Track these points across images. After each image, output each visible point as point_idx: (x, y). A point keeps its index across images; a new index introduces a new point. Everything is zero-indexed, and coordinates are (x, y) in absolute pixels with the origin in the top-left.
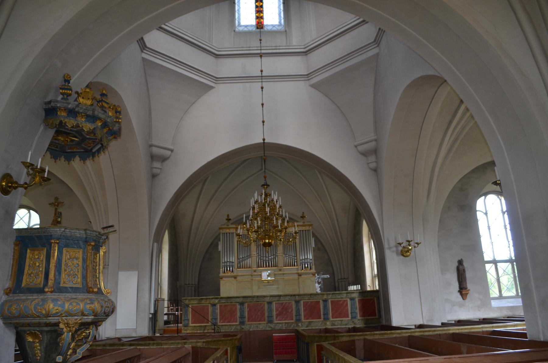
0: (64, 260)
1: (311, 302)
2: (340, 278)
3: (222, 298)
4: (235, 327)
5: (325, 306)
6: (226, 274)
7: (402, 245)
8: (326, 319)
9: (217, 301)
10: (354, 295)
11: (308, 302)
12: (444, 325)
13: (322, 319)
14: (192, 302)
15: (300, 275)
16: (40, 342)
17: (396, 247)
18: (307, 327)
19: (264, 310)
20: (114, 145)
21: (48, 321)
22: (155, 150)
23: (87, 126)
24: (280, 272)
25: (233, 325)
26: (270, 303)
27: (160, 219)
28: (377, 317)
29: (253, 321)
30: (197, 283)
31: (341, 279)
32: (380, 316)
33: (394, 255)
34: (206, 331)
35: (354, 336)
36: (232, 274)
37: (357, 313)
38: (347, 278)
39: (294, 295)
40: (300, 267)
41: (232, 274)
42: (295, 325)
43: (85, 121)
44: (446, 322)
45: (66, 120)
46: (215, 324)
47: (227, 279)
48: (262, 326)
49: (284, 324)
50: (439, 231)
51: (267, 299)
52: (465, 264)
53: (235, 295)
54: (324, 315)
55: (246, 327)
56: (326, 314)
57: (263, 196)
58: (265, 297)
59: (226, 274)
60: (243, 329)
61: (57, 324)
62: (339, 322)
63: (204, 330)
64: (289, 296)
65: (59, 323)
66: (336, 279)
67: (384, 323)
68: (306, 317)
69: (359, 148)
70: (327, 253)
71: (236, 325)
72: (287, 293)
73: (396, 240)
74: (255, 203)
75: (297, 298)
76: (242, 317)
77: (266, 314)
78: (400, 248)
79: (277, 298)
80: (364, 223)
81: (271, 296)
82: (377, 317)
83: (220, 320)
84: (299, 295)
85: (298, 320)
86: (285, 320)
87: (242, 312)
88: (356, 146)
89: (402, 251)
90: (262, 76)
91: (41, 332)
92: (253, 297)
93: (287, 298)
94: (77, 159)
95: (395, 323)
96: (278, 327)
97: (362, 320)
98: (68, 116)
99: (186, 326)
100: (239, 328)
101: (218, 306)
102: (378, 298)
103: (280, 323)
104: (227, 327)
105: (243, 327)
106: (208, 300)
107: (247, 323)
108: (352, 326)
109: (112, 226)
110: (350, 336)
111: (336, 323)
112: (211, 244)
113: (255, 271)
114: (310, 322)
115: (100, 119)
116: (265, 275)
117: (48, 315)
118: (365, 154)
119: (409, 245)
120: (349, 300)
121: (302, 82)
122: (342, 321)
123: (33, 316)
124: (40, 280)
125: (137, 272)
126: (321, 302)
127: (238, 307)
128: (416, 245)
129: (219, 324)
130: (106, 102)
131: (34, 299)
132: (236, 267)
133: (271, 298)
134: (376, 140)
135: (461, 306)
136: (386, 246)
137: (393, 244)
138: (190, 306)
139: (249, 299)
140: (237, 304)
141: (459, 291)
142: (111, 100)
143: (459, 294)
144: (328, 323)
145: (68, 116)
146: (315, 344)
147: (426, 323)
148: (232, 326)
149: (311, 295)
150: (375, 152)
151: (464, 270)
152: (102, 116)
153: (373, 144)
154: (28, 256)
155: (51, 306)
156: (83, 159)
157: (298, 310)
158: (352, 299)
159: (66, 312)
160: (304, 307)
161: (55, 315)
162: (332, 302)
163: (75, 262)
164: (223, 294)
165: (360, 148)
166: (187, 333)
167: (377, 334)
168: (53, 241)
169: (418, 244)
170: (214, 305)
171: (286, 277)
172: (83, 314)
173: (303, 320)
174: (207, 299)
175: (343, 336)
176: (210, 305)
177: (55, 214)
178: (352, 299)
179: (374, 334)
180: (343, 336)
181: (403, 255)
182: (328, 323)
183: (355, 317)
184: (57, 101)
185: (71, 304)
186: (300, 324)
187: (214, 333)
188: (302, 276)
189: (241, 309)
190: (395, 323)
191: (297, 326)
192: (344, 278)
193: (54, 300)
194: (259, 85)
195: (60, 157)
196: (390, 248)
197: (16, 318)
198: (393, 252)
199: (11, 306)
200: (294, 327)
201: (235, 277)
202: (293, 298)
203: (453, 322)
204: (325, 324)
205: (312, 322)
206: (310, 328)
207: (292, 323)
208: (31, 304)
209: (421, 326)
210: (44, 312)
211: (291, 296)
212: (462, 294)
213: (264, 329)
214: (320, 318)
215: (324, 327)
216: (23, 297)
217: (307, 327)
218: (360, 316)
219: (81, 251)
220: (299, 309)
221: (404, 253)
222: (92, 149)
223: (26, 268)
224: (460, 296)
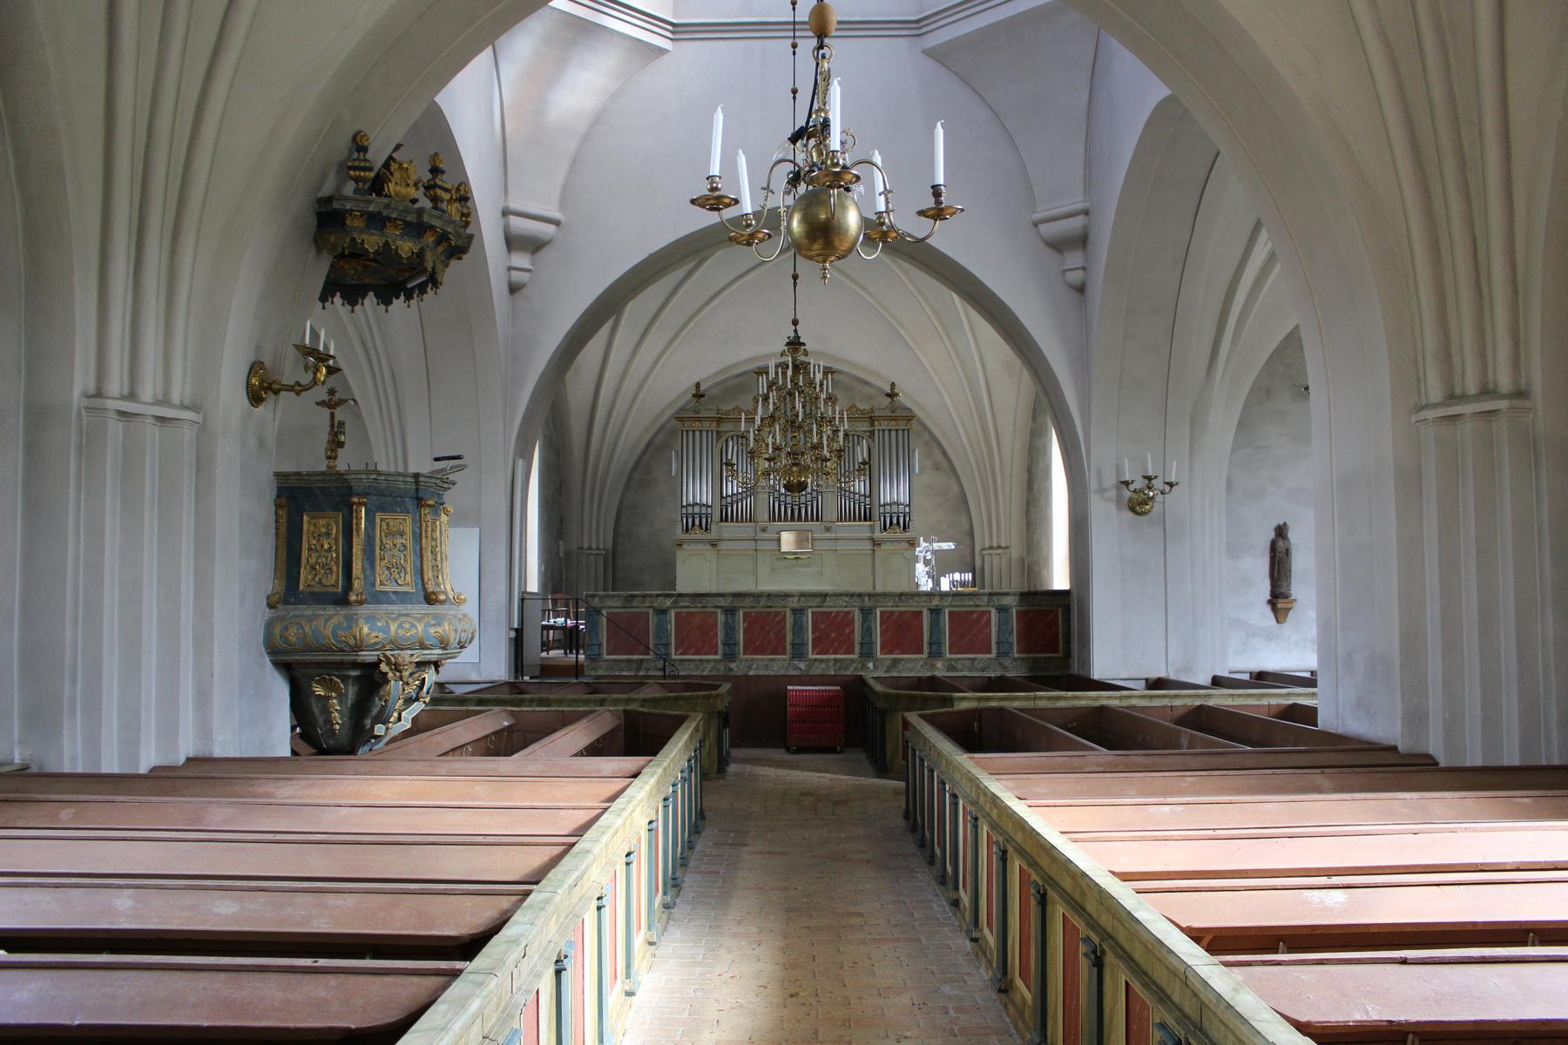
1: (902, 614)
3: (680, 595)
5: (935, 624)
6: (693, 536)
7: (1132, 487)
8: (935, 654)
9: (668, 602)
10: (1006, 601)
11: (892, 613)
12: (1217, 682)
13: (925, 655)
14: (608, 603)
15: (876, 543)
16: (341, 697)
17: (1118, 488)
18: (888, 670)
20: (454, 272)
21: (360, 659)
22: (517, 223)
23: (406, 247)
24: (828, 535)
27: (531, 400)
28: (1060, 655)
29: (758, 651)
30: (610, 545)
31: (991, 548)
32: (1068, 655)
33: (1112, 507)
34: (642, 673)
35: (988, 699)
36: (707, 536)
37: (1011, 644)
39: (860, 595)
41: (707, 536)
43: (402, 235)
44: (1226, 675)
45: (364, 237)
46: (665, 658)
47: (693, 547)
48: (774, 665)
50: (1233, 451)
51: (794, 603)
52: (1293, 536)
53: (714, 590)
54: (930, 644)
55: (737, 668)
56: (935, 643)
57: (790, 373)
58: (787, 595)
59: (693, 536)
61: (376, 665)
62: (967, 663)
63: (639, 669)
65: (380, 661)
67: (1075, 669)
69: (1044, 228)
70: (958, 478)
73: (1119, 469)
74: (770, 388)
75: (867, 602)
76: (730, 642)
78: (1127, 494)
81: (803, 595)
82: (1060, 655)
84: (870, 595)
85: (867, 653)
86: (836, 653)
87: (730, 630)
88: (1036, 224)
89: (1130, 500)
90: (794, 23)
91: (345, 679)
92: (758, 596)
93: (841, 602)
94: (370, 299)
95: (1098, 672)
96: (816, 671)
97: (1023, 659)
98: (368, 226)
99: (594, 659)
102: (1067, 609)
103: (821, 661)
105: (733, 665)
107: (742, 656)
108: (999, 674)
109: (458, 457)
110: (979, 699)
111: (959, 666)
112: (648, 445)
113: (764, 530)
115: (432, 228)
116: (788, 540)
117: (358, 648)
118: (1058, 245)
119: (1150, 488)
120: (993, 612)
121: (903, 41)
122: (973, 660)
123: (328, 649)
124: (335, 579)
125: (477, 530)
126: (925, 613)
127: (721, 618)
128: (1167, 488)
130: (442, 188)
131: (330, 617)
132: (717, 517)
134: (1086, 213)
135: (1270, 637)
136: (1093, 485)
137: (1110, 480)
138: (604, 612)
139: (747, 602)
141: (1269, 602)
142: (448, 180)
143: (1268, 609)
144: (939, 664)
145: (368, 226)
147: (1172, 677)
148: (705, 664)
149: (901, 595)
150: (1081, 241)
151: (1288, 552)
152: (437, 223)
153: (1077, 223)
154: (305, 527)
155: (366, 630)
156: (386, 299)
157: (867, 631)
158: (1002, 610)
159: (392, 642)
161: (373, 647)
163: (399, 541)
164: (684, 585)
165: (1048, 230)
166: (598, 677)
167: (1041, 698)
168: (355, 500)
169: (1171, 485)
170: (664, 612)
171: (841, 546)
172: (423, 646)
174: (645, 596)
175: (963, 699)
177: (332, 426)
178: (1002, 610)
179: (1035, 698)
180: (963, 699)
181: (1133, 510)
182: (939, 664)
183: (1006, 654)
184: (346, 199)
185: (400, 626)
186: (871, 665)
187: (664, 677)
189: (726, 623)
190: (1097, 674)
191: (864, 667)
192: (999, 547)
193: (371, 619)
194: (790, 41)
195: (333, 296)
196: (1102, 491)
197: (296, 652)
198: (1109, 500)
199: (286, 629)
201: (714, 544)
202: (857, 602)
203: (1246, 677)
204: (933, 666)
207: (852, 661)
208: (325, 624)
209: (1157, 684)
210: (352, 642)
211: (852, 595)
212: (1275, 609)
216: (307, 611)
217: (888, 670)
218: (1019, 652)
219: (409, 521)
220: (801, 626)
221: (1138, 505)
222: (405, 282)
223: (305, 554)
224: (1270, 614)
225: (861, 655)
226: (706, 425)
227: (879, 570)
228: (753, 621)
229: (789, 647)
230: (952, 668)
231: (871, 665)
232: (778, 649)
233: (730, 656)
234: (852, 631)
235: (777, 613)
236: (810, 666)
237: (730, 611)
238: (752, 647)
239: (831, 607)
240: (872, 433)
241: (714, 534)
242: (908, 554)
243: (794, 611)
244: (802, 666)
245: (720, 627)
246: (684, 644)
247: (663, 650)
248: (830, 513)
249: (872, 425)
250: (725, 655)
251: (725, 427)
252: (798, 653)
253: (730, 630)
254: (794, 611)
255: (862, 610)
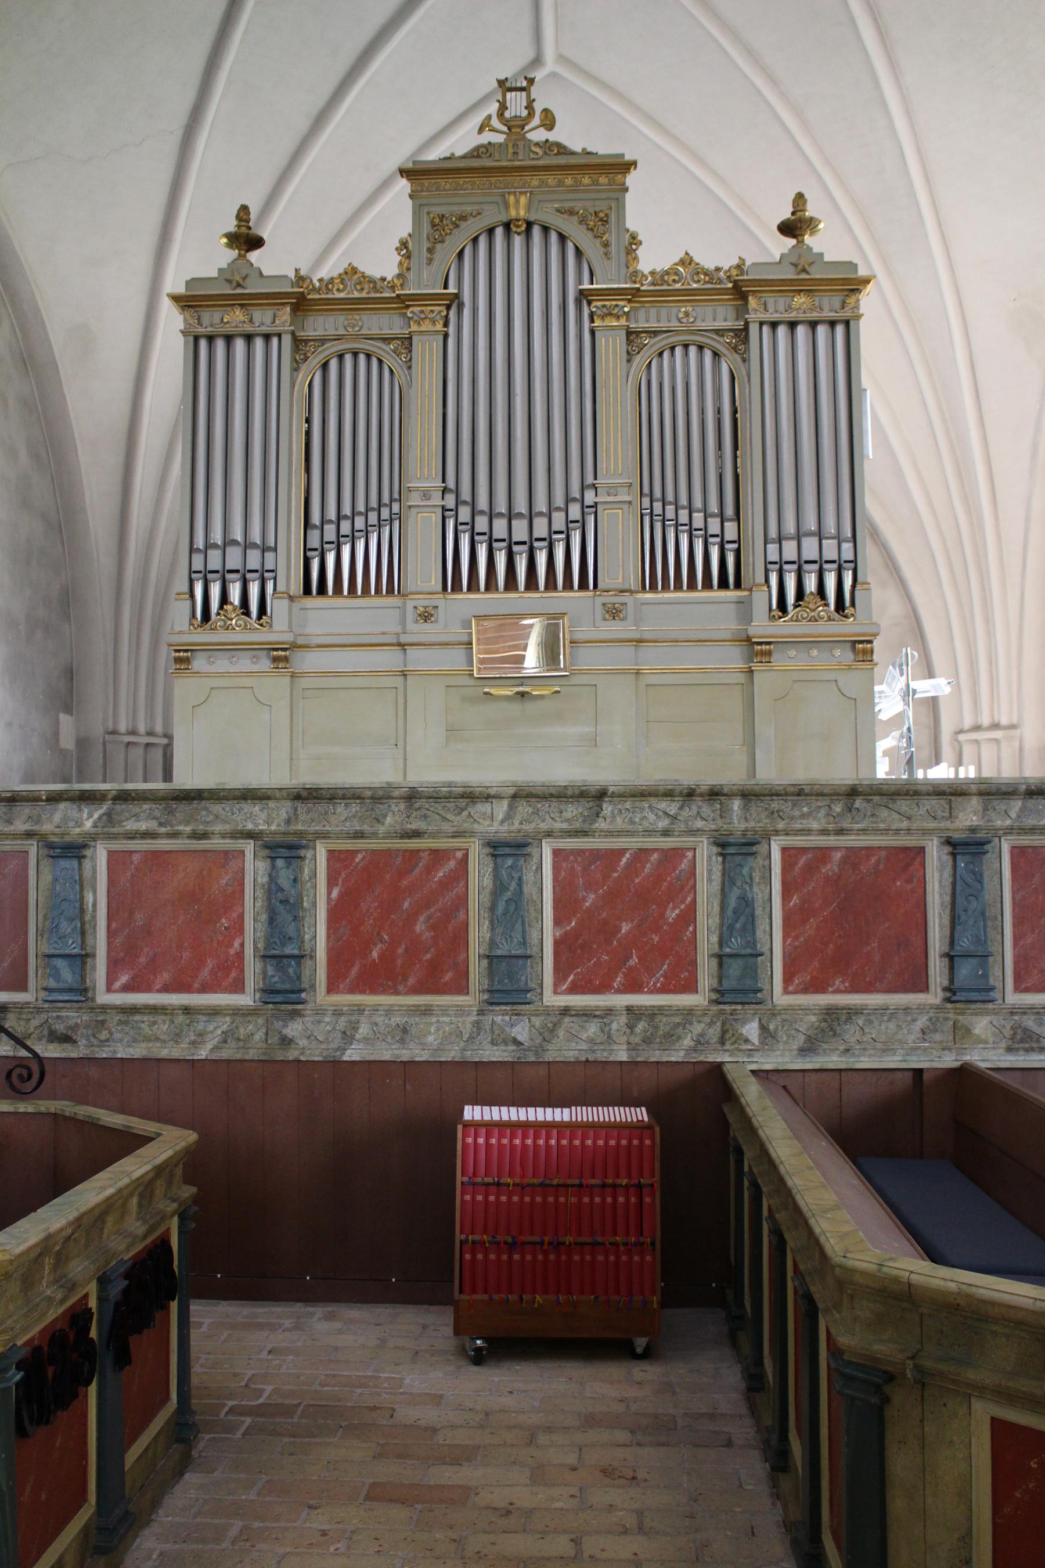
0: (565, 826)
1: (854, 857)
2: (968, 723)
4: (224, 1023)
8: (967, 993)
9: (88, 819)
11: (823, 854)
13: (934, 997)
18: (809, 1048)
19: (463, 901)
25: (214, 1012)
26: (509, 851)
29: (374, 979)
31: (977, 728)
38: (1012, 727)
39: (714, 794)
40: (763, 600)
42: (714, 1032)
47: (222, 663)
49: (618, 1024)
51: (495, 820)
55: (310, 1037)
58: (470, 796)
60: (286, 1042)
64: (669, 794)
66: (947, 728)
68: (809, 969)
71: (236, 1012)
72: (652, 775)
75: (738, 819)
76: (284, 956)
77: (478, 935)
79: (572, 810)
80: (93, 1389)
81: (521, 795)
83: (114, 966)
84: (748, 795)
85: (739, 992)
86: (633, 986)
93: (653, 816)
96: (569, 1046)
100: (256, 1032)
101: (100, 856)
103: (587, 1014)
104: (163, 1027)
106: (25, 810)
107: (321, 996)
113: (426, 616)
114: (831, 1014)
126: (935, 855)
127: (255, 868)
129: (103, 998)
133: (524, 809)
139: (342, 817)
140: (249, 847)
144: (981, 1025)
146: (983, 1412)
157: (740, 916)
160: (787, 892)
162: (1018, 853)
170: (73, 850)
171: (651, 658)
173: (780, 998)
176: (33, 849)
188: (779, 660)
189: (273, 889)
192: (995, 726)
200: (700, 1042)
201: (281, 656)
202: (703, 817)
204: (961, 1033)
205: (853, 1012)
206: (833, 1060)
207: (689, 1013)
211: (690, 794)
213: (452, 1054)
214: (918, 982)
215: (949, 1061)
217: (809, 1048)
220: (746, 903)
225: (721, 995)
226: (262, 318)
227: (765, 731)
228: (364, 881)
229: (476, 969)
230: (1022, 1039)
231: (751, 1030)
232: (441, 973)
233: (284, 996)
234: (689, 915)
235: (438, 856)
236: (548, 1033)
237: (286, 850)
238: (362, 966)
239: (619, 832)
240: (742, 334)
241: (282, 623)
242: (851, 682)
243: (496, 848)
244: (521, 1031)
245: (252, 905)
246: (134, 963)
247: (68, 976)
248: (620, 564)
249: (742, 309)
250: (268, 992)
251: (317, 326)
252: (509, 989)
253: (284, 907)
254: (496, 848)
255: (722, 844)
